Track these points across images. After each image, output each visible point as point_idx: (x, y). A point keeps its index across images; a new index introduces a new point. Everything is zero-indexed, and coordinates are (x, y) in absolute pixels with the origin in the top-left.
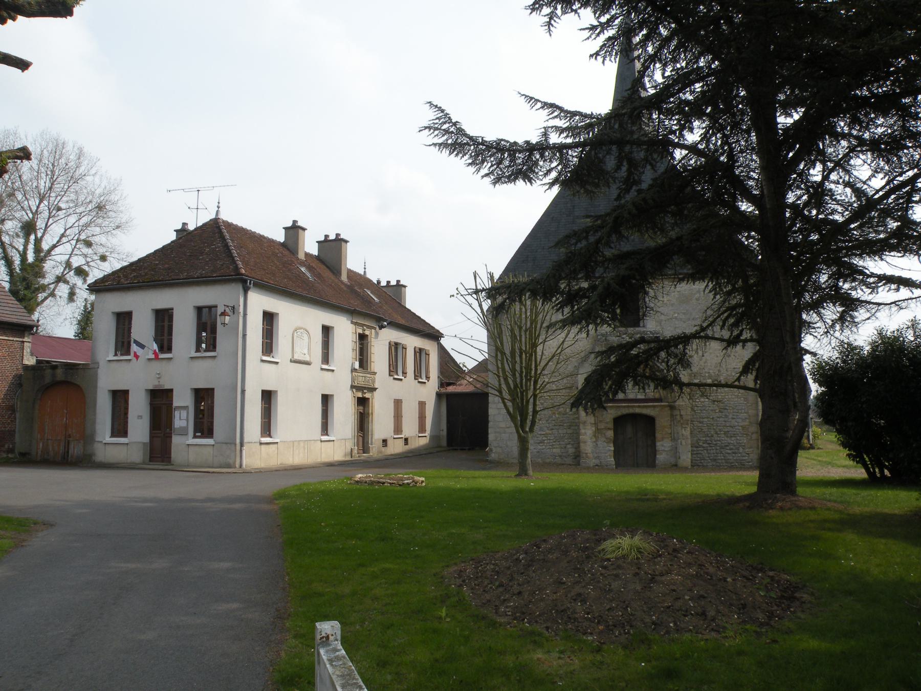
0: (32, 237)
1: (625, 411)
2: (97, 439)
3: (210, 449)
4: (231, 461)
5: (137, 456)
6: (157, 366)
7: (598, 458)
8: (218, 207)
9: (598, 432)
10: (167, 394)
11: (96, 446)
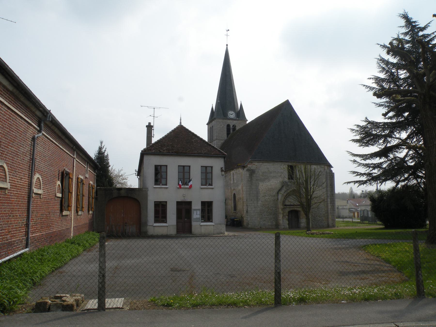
0: (371, 172)
1: (292, 209)
2: (149, 224)
3: (212, 227)
4: (223, 231)
5: (173, 231)
6: (182, 191)
7: (284, 225)
8: (181, 120)
9: (284, 216)
10: (189, 203)
11: (148, 227)
